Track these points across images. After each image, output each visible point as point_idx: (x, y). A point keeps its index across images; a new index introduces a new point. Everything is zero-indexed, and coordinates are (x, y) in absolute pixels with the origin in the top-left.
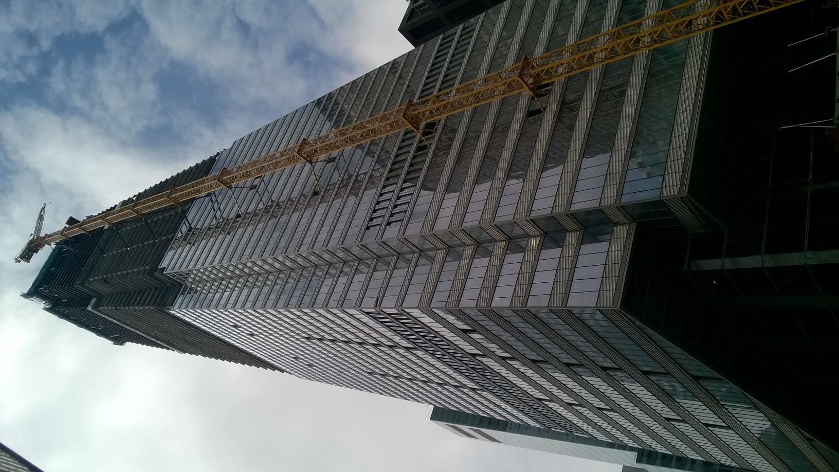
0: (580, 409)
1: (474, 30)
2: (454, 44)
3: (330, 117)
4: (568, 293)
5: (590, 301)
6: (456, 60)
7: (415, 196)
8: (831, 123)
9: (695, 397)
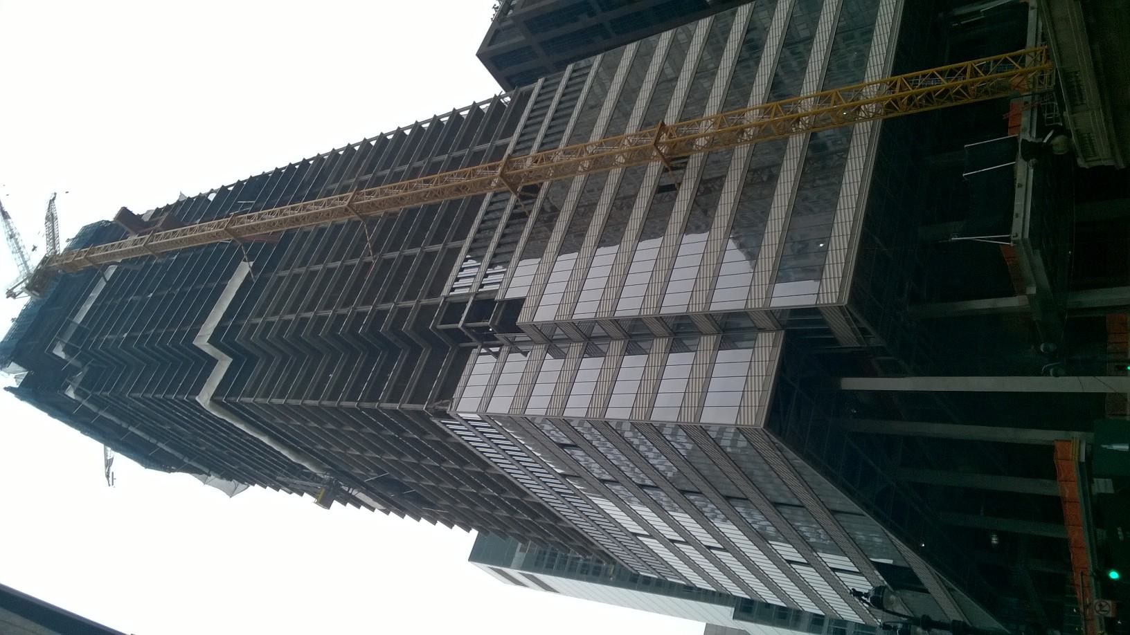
2: (560, 90)
4: (701, 406)
5: (728, 418)
6: (562, 110)
8: (1008, 240)
9: (787, 541)
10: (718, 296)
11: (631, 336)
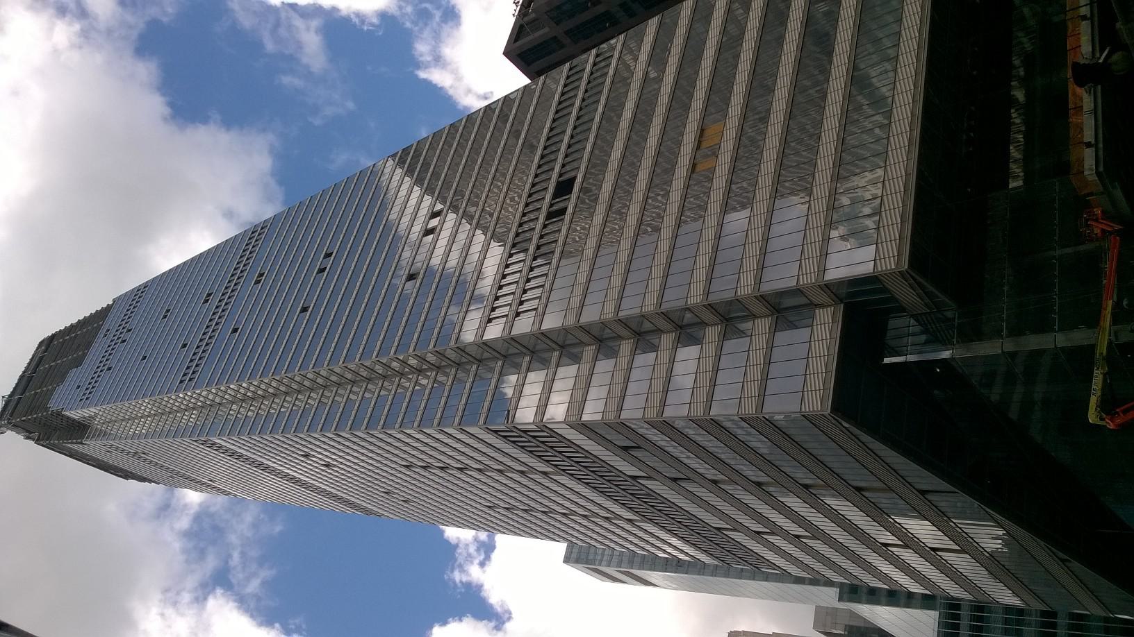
0: (771, 538)
1: (584, 70)
3: (410, 172)
7: (551, 276)
10: (768, 275)
11: (727, 320)
